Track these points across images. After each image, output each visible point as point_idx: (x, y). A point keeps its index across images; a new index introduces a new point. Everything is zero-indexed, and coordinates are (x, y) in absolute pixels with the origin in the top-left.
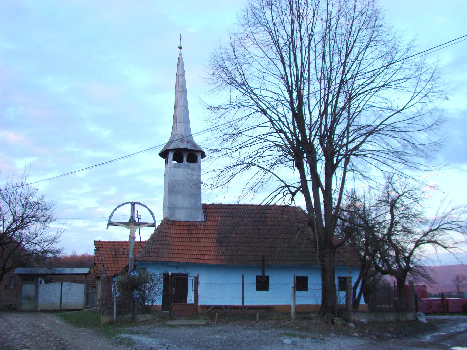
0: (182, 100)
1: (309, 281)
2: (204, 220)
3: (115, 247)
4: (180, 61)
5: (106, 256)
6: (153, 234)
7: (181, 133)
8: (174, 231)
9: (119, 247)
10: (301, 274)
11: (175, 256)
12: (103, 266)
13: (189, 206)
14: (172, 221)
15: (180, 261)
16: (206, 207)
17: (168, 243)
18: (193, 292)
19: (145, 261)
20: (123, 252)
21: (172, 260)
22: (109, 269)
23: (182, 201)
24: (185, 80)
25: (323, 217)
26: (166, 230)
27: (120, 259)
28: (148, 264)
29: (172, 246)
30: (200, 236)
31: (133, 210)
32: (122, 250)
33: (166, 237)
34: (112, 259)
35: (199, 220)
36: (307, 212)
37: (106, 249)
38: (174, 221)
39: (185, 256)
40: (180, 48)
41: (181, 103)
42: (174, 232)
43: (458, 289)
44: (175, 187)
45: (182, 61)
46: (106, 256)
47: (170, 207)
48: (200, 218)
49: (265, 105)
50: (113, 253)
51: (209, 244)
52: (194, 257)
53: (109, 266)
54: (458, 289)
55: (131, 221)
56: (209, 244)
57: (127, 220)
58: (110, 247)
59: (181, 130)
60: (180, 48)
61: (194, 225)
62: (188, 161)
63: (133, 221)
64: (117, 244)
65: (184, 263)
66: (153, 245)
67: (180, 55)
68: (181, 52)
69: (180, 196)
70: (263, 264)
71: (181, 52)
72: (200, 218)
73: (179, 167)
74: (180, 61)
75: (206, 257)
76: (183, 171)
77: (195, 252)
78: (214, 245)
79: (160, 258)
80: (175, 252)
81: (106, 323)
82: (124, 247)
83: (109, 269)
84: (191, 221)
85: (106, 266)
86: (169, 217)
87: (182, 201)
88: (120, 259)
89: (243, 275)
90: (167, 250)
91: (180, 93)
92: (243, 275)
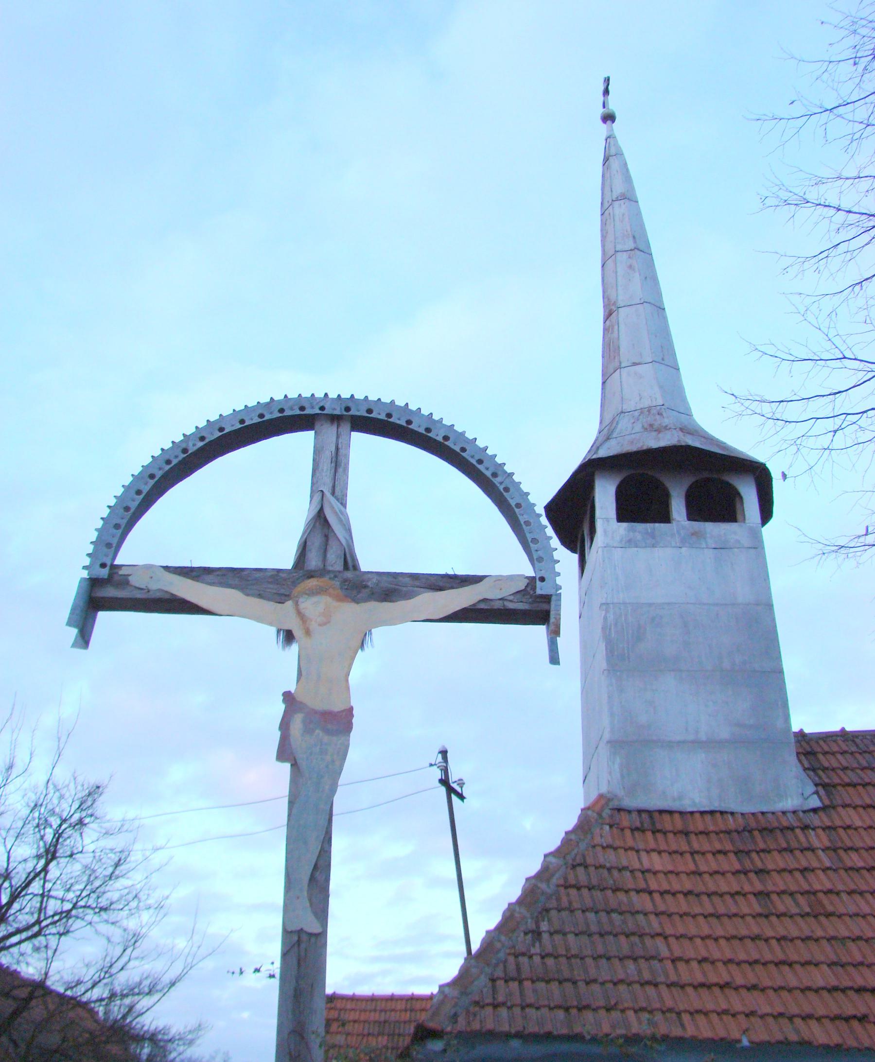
0: (637, 278)
2: (815, 802)
3: (393, 1016)
4: (611, 156)
6: (539, 876)
7: (646, 403)
8: (657, 862)
11: (694, 999)
13: (724, 733)
14: (640, 811)
15: (735, 1034)
16: (813, 750)
17: (631, 926)
19: (491, 1035)
21: (677, 1032)
23: (685, 709)
24: (639, 214)
26: (610, 858)
29: (659, 942)
30: (820, 882)
31: (330, 478)
33: (616, 890)
35: (790, 803)
38: (649, 812)
39: (761, 1004)
40: (609, 118)
41: (631, 289)
42: (658, 867)
43: (670, 745)
45: (619, 154)
48: (794, 793)
52: (819, 1005)
54: (670, 745)
55: (313, 561)
57: (284, 559)
58: (374, 1016)
59: (641, 388)
61: (771, 831)
62: (691, 517)
63: (334, 561)
64: (400, 1006)
65: (759, 1047)
66: (537, 934)
72: (794, 793)
73: (653, 542)
77: (820, 977)
79: (589, 1015)
80: (686, 978)
84: (748, 809)
86: (621, 793)
87: (685, 709)
90: (631, 966)
91: (622, 257)
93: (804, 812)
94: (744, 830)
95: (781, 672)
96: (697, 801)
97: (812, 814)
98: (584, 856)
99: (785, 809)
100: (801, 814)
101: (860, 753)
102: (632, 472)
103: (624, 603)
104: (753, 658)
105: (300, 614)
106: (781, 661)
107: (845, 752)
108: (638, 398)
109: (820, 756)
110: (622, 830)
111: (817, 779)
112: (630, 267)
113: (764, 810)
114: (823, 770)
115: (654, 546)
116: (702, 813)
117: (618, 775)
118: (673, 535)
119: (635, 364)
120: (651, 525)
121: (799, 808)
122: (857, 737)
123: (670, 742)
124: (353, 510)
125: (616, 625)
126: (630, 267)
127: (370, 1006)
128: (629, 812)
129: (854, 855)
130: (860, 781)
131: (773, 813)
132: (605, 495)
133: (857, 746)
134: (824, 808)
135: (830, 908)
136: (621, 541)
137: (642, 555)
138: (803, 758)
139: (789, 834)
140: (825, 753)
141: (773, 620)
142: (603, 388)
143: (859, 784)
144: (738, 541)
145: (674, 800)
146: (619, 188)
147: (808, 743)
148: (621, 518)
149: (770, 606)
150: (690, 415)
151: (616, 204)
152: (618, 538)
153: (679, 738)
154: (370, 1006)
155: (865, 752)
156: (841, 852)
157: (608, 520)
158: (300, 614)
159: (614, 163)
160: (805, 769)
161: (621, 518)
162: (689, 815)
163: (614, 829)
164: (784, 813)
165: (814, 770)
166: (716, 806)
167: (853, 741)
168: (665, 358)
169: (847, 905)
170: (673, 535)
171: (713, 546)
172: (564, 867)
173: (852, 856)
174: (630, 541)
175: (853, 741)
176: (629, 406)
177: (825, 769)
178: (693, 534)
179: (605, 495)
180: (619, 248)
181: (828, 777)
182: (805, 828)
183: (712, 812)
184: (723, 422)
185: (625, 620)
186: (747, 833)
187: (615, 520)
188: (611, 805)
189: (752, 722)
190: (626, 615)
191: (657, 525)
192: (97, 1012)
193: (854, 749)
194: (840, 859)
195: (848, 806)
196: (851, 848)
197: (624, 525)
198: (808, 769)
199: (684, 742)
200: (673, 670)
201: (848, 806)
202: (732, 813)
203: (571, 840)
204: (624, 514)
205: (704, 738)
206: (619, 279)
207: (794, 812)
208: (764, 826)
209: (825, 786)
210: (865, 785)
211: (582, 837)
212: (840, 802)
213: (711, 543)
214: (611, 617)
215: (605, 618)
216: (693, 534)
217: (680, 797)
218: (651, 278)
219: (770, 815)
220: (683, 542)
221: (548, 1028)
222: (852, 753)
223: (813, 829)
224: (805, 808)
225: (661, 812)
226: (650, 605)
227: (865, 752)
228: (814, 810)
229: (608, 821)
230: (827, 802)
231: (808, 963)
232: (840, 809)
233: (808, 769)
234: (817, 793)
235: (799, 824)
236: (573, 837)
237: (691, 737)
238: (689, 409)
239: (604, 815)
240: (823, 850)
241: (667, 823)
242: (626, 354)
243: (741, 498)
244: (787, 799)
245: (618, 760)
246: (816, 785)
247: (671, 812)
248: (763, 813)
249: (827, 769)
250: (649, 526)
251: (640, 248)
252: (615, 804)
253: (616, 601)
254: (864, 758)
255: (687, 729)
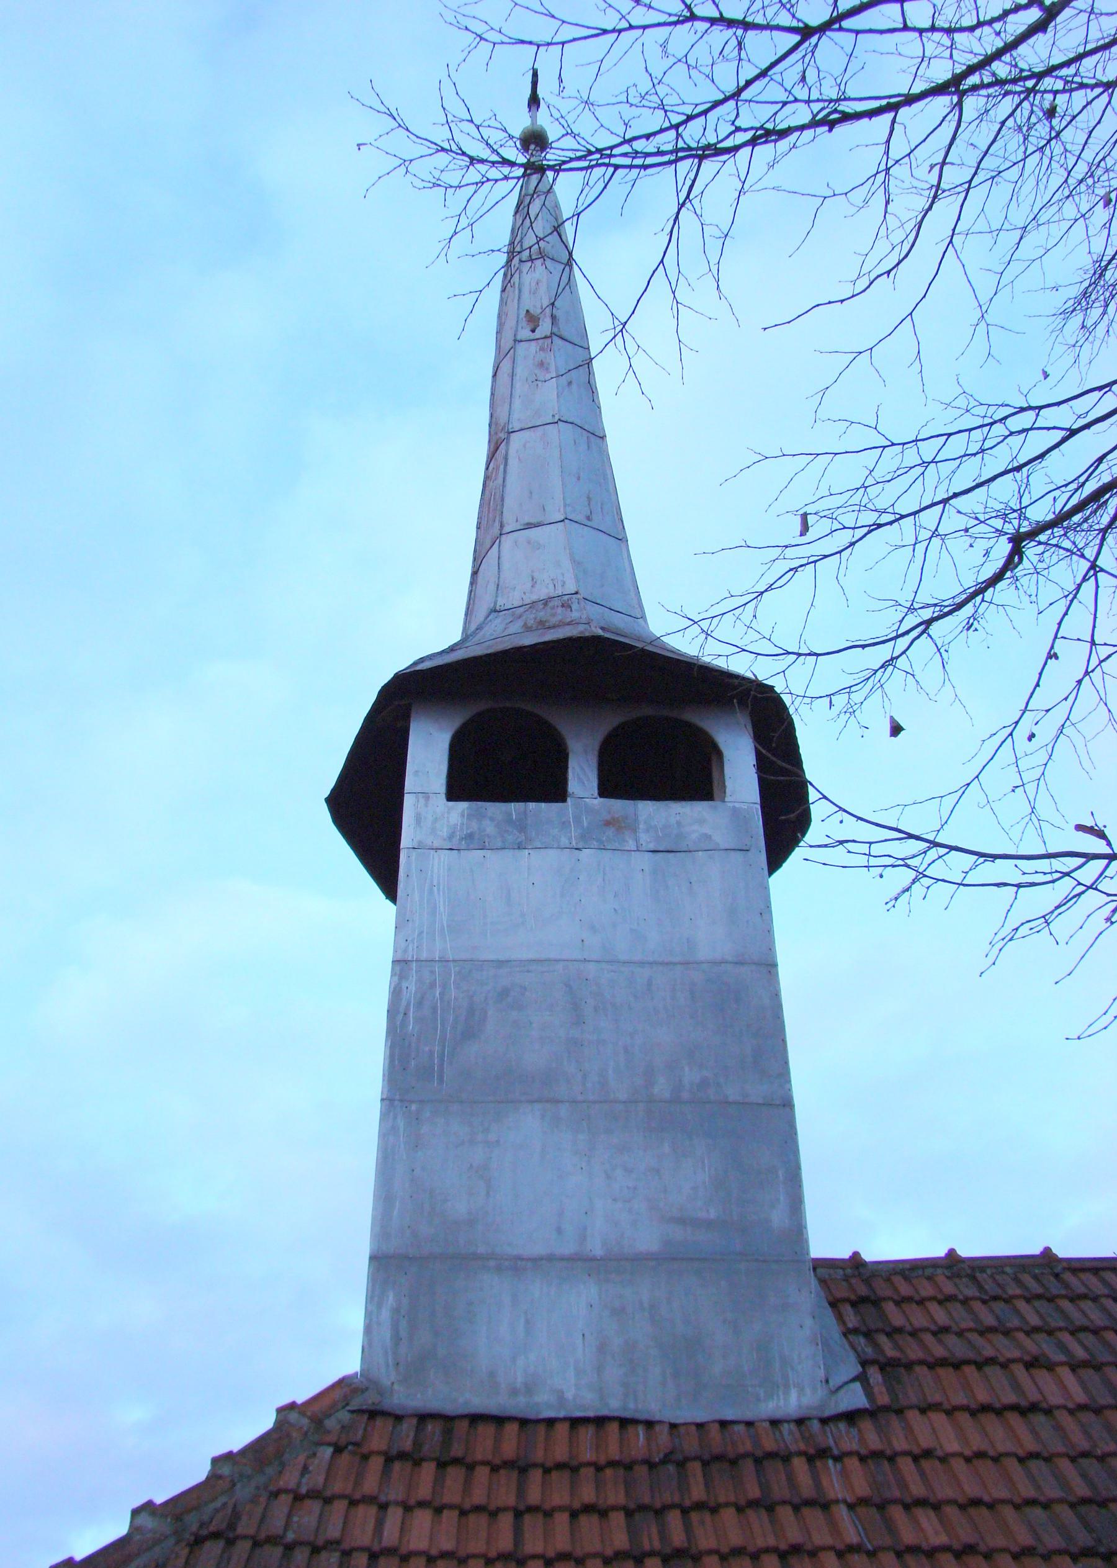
2: (854, 1398)
13: (647, 1239)
14: (423, 1418)
23: (562, 1185)
25: (665, 712)
35: (792, 1401)
36: (481, 706)
38: (447, 1420)
43: (517, 1266)
44: (470, 1030)
47: (420, 1264)
48: (803, 1374)
49: (861, 99)
54: (517, 1266)
62: (612, 785)
69: (527, 1126)
76: (562, 884)
86: (387, 1376)
87: (562, 1185)
93: (824, 1421)
94: (666, 1460)
95: (787, 1104)
96: (569, 1395)
97: (842, 1426)
98: (236, 1515)
99: (779, 1414)
100: (815, 1425)
101: (984, 1302)
103: (444, 961)
104: (727, 1076)
106: (789, 1081)
107: (950, 1298)
108: (529, 584)
109: (890, 1308)
110: (365, 1457)
111: (869, 1350)
113: (729, 1414)
114: (888, 1334)
115: (520, 847)
116: (576, 1422)
117: (387, 1334)
118: (565, 825)
119: (529, 526)
120: (522, 804)
121: (815, 1413)
122: (982, 1269)
123: (519, 1258)
125: (420, 1004)
126: (541, 364)
128: (398, 1418)
129: (927, 1519)
130: (971, 1355)
131: (749, 1424)
132: (428, 754)
133: (981, 1288)
134: (872, 1413)
136: (451, 837)
137: (495, 865)
138: (848, 1310)
139: (774, 1470)
140: (901, 1301)
141: (776, 996)
142: (473, 582)
143: (968, 1362)
144: (708, 837)
145: (514, 1392)
147: (867, 1281)
148: (453, 794)
149: (769, 967)
152: (445, 833)
153: (540, 1250)
155: (995, 1298)
156: (897, 1513)
157: (426, 796)
160: (846, 1334)
161: (453, 794)
162: (542, 1429)
163: (345, 1457)
164: (775, 1423)
165: (868, 1334)
166: (614, 1406)
167: (973, 1278)
168: (597, 515)
170: (565, 825)
171: (652, 847)
172: (172, 1540)
173: (924, 1523)
174: (470, 837)
175: (973, 1278)
177: (893, 1332)
178: (608, 824)
179: (428, 754)
181: (899, 1348)
182: (818, 1455)
183: (600, 1421)
185: (442, 994)
186: (671, 1468)
187: (444, 796)
188: (355, 1404)
189: (713, 1214)
190: (444, 986)
191: (532, 805)
193: (971, 1291)
194: (891, 1527)
195: (936, 1407)
196: (922, 1502)
197: (463, 806)
198: (855, 1331)
199: (550, 1258)
200: (539, 1101)
201: (936, 1407)
202: (649, 1424)
203: (220, 1477)
204: (463, 784)
205: (598, 1252)
206: (518, 385)
207: (800, 1422)
208: (717, 1450)
209: (887, 1366)
210: (980, 1365)
211: (248, 1470)
212: (914, 1399)
213: (646, 840)
216: (608, 824)
217: (529, 1388)
219: (741, 1428)
220: (586, 839)
222: (965, 1302)
223: (837, 1459)
224: (827, 1413)
225: (475, 1419)
226: (501, 963)
227: (995, 1298)
228: (850, 1417)
229: (332, 1438)
230: (884, 1399)
232: (913, 1416)
233: (855, 1331)
234: (862, 1378)
235: (802, 1446)
236: (226, 1470)
237: (569, 1249)
239: (331, 1423)
240: (851, 1507)
242: (513, 512)
244: (786, 1393)
245: (391, 1299)
246: (864, 1363)
247: (499, 1420)
248: (724, 1424)
249: (899, 1330)
250: (514, 808)
253: (424, 955)
254: (992, 1311)
255: (559, 1231)
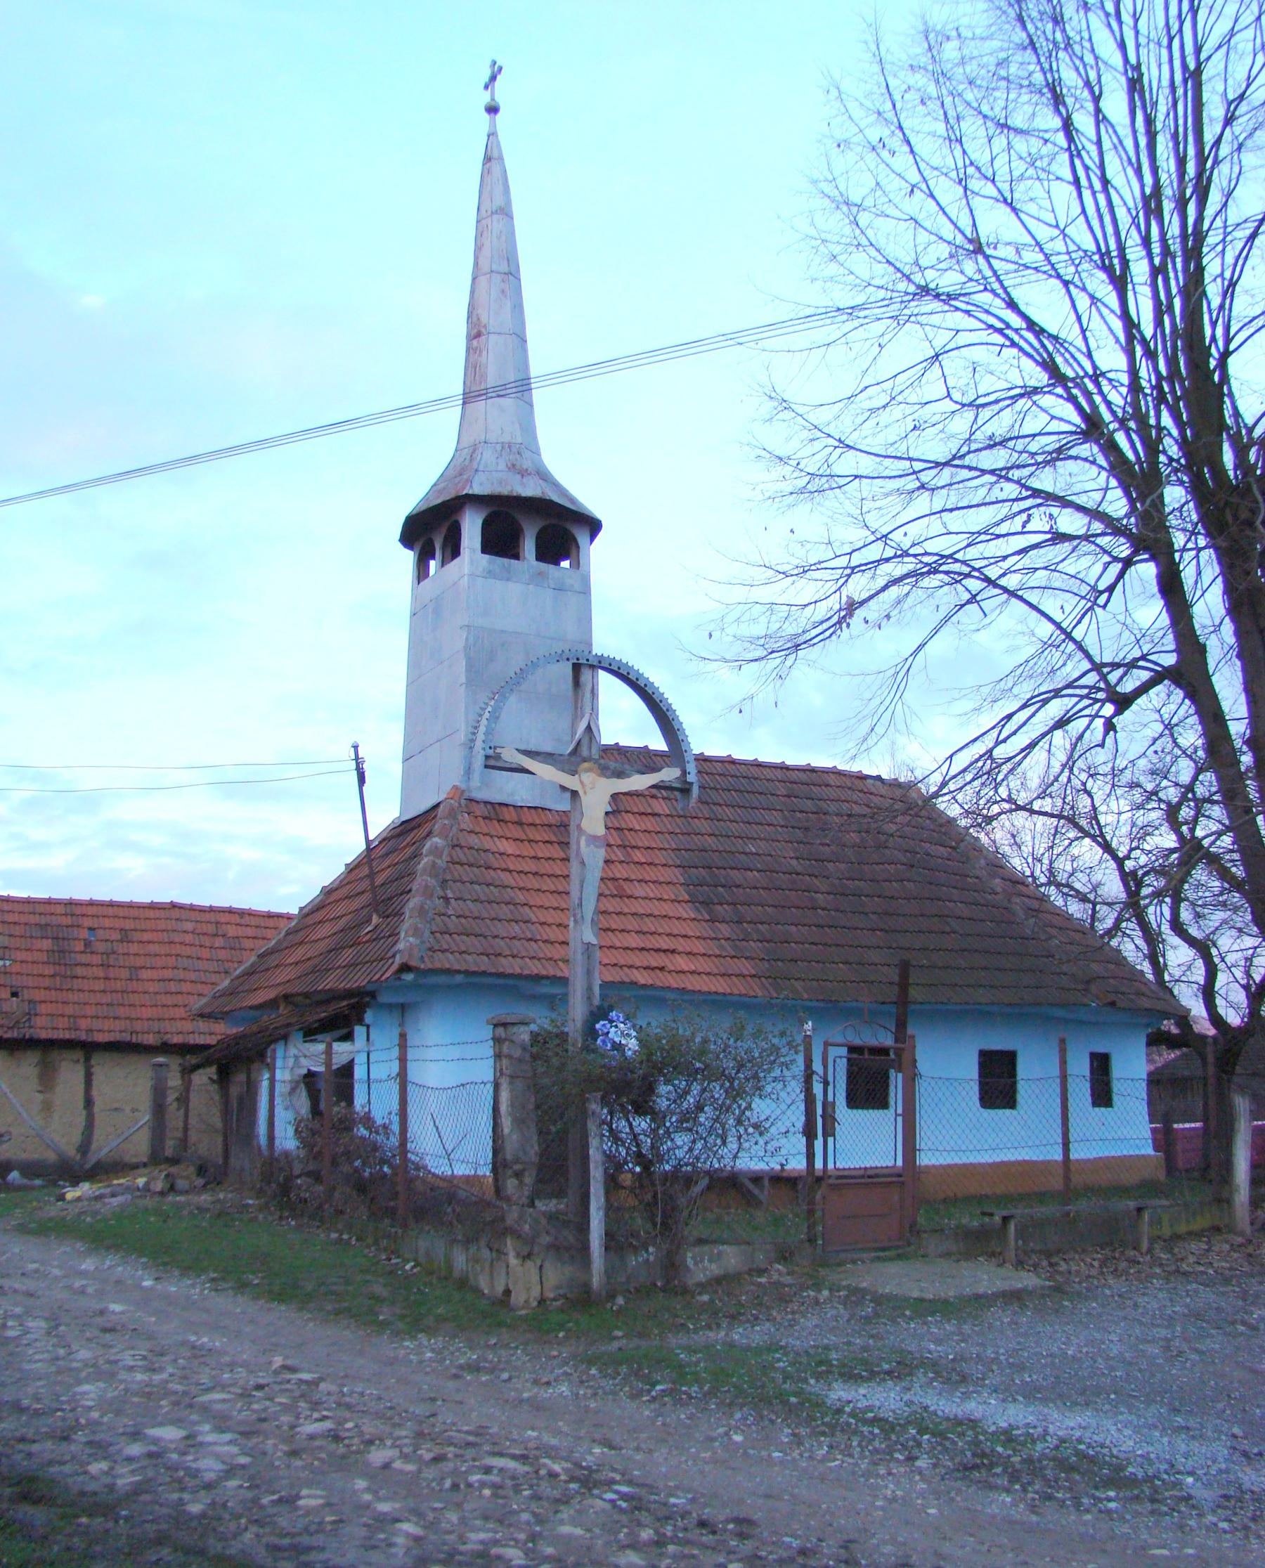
1: (1022, 1070)
3: (54, 920)
4: (492, 158)
5: (21, 956)
7: (506, 438)
8: (504, 846)
9: (68, 921)
10: (997, 1042)
12: (15, 994)
14: (486, 803)
18: (900, 1119)
20: (87, 944)
22: (43, 1009)
24: (512, 233)
27: (79, 971)
28: (434, 989)
32: (84, 934)
34: (48, 970)
37: (18, 930)
40: (492, 110)
46: (21, 956)
50: (46, 944)
51: (668, 909)
53: (42, 995)
56: (668, 909)
58: (33, 919)
60: (492, 110)
62: (541, 557)
67: (492, 135)
68: (493, 124)
70: (903, 1001)
71: (493, 124)
73: (507, 577)
74: (492, 158)
75: (681, 962)
77: (633, 941)
78: (685, 911)
81: (542, 1301)
82: (87, 922)
83: (43, 1009)
85: (26, 994)
88: (79, 971)
89: (1062, 1041)
92: (1062, 1041)
102: (496, 509)
105: (582, 783)
112: (503, 292)
115: (508, 580)
124: (601, 722)
127: (27, 908)
132: (471, 527)
135: (629, 893)
146: (499, 202)
150: (539, 455)
151: (495, 217)
154: (27, 908)
158: (582, 783)
159: (495, 167)
169: (639, 890)
176: (492, 437)
179: (471, 527)
180: (495, 267)
183: (535, 808)
184: (575, 474)
192: (1169, 1032)
194: (629, 855)
197: (487, 556)
214: (471, 639)
215: (467, 639)
218: (518, 308)
221: (483, 968)
231: (623, 931)
238: (538, 448)
241: (508, 815)
243: (578, 547)
247: (507, 805)
250: (506, 561)
251: (511, 274)
252: (466, 795)
